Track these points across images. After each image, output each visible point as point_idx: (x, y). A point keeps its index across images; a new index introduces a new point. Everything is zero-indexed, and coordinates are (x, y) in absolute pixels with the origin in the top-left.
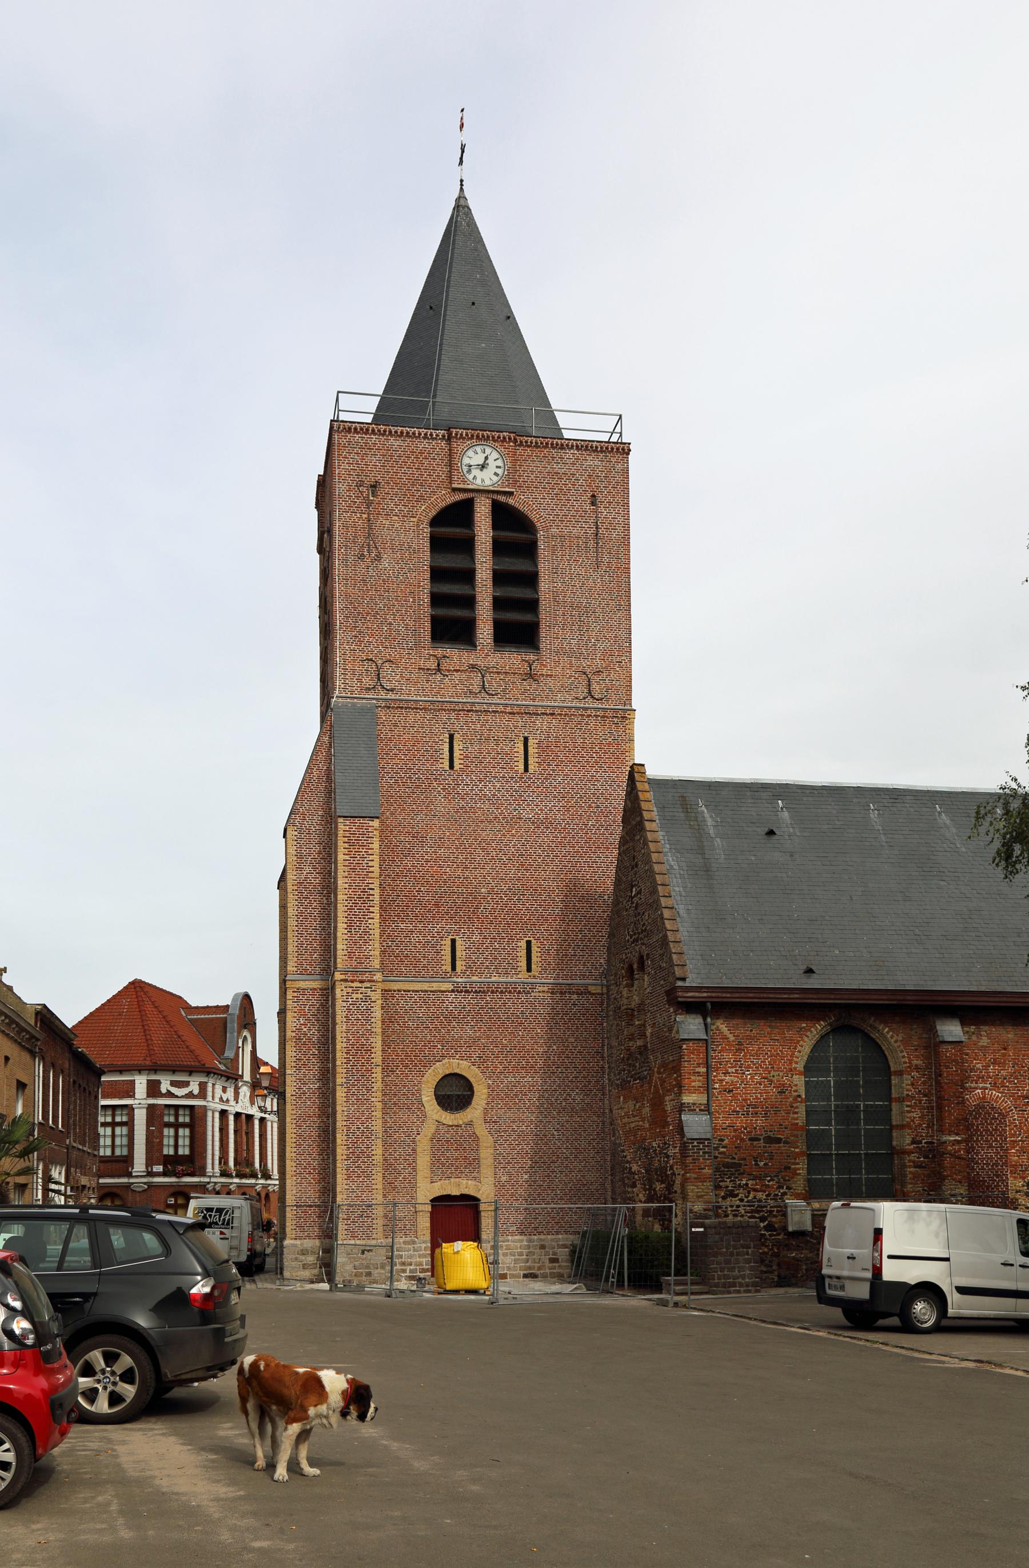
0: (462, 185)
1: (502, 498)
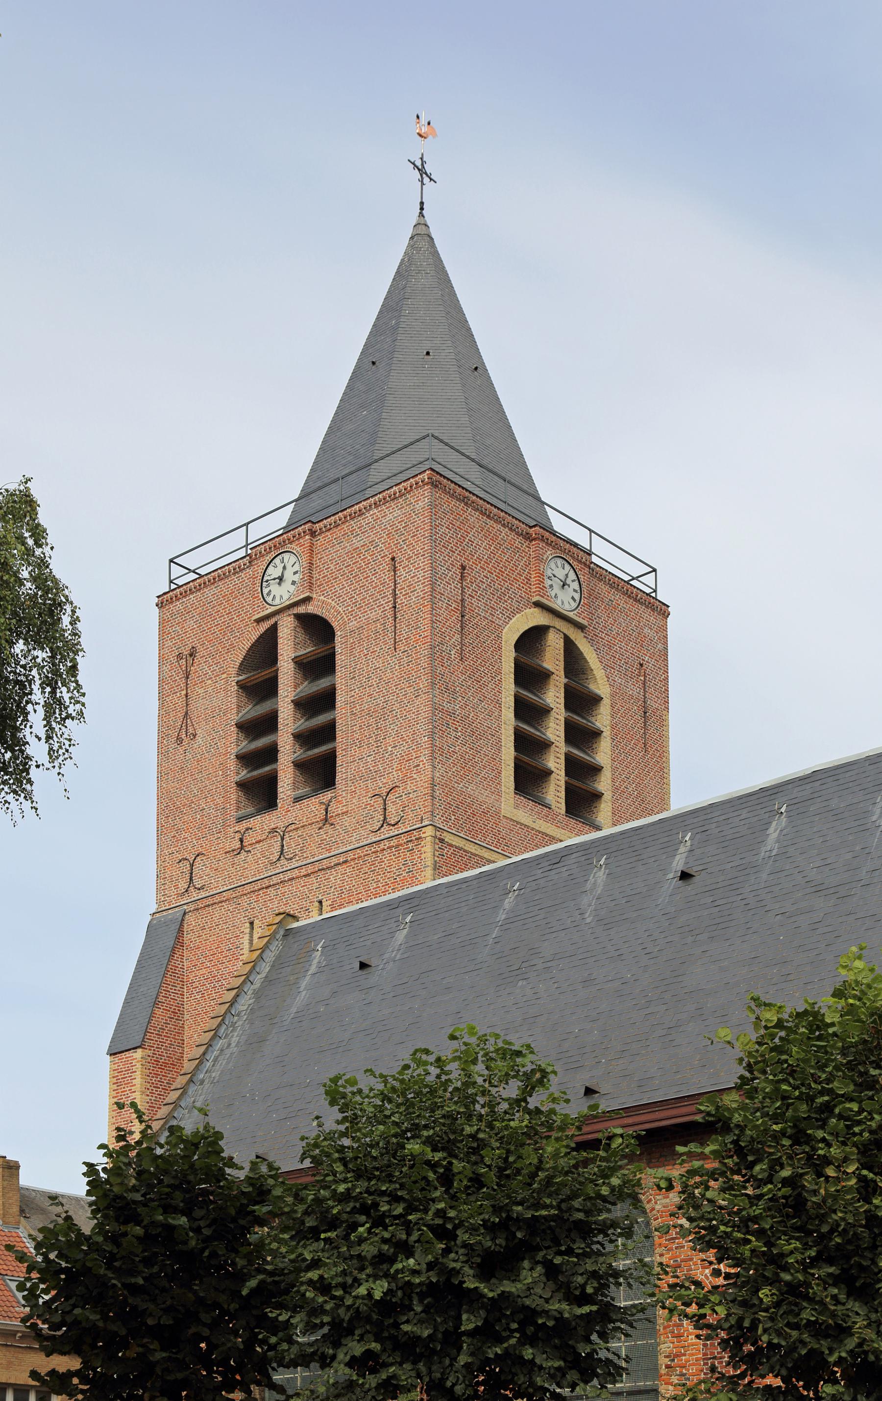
0: (422, 209)
1: (301, 610)
